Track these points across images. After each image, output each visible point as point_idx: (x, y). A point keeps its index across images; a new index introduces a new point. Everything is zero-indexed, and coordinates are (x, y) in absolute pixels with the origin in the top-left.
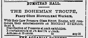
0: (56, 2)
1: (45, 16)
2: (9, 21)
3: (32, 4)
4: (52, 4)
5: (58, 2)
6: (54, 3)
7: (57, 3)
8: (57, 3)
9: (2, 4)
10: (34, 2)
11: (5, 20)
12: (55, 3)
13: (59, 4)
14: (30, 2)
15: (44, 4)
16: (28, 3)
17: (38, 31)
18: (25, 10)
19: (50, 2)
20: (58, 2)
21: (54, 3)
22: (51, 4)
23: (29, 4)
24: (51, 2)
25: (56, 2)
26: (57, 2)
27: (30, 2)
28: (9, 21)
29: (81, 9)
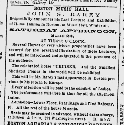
0: (83, 8)
1: (41, 103)
2: (79, 115)
3: (10, 122)
4: (79, 9)
5: (86, 8)
6: (80, 8)
7: (85, 9)
8: (85, 9)
9: (6, 40)
10: (59, 8)
11: (11, 18)
12: (82, 9)
13: (88, 11)
14: (35, 123)
15: (81, 11)
16: (35, 8)
17: (95, 57)
18: (95, 77)
19: (76, 8)
20: (86, 8)
21: (80, 8)
22: (77, 10)
23: (36, 10)
24: (78, 8)
25: (83, 8)
26: (85, 8)
27: (35, 123)
28: (79, 115)
29: (113, 12)
